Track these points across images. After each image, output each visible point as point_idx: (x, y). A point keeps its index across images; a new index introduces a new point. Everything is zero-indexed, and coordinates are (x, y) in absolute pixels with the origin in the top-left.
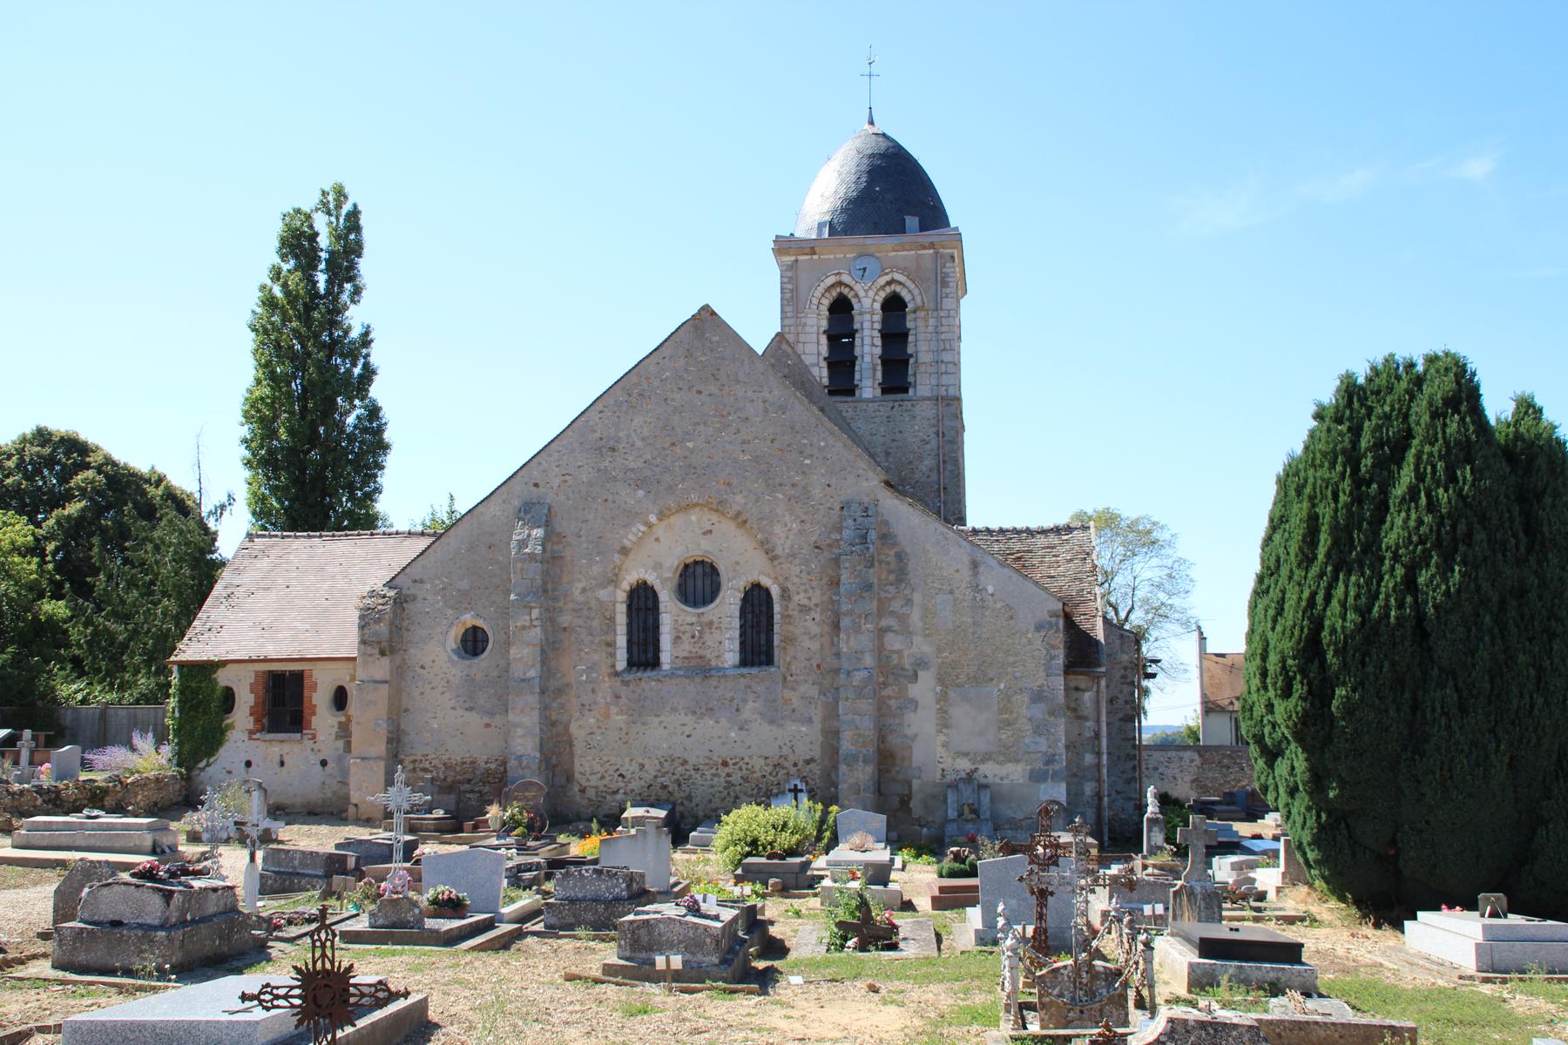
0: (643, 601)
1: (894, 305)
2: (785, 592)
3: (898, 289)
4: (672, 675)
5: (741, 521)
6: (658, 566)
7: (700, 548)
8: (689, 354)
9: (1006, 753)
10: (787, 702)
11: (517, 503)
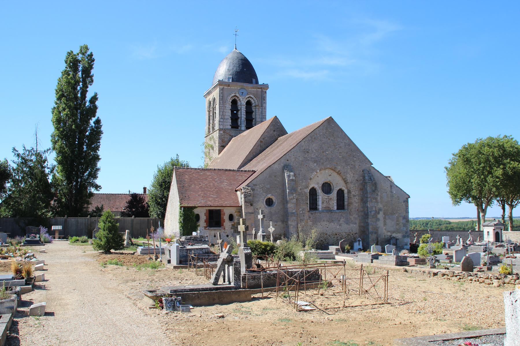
0: (313, 192)
1: (249, 103)
2: (349, 192)
3: (251, 99)
4: (323, 211)
5: (339, 173)
6: (318, 183)
7: (328, 179)
8: (327, 129)
9: (397, 231)
10: (351, 219)
11: (282, 165)
